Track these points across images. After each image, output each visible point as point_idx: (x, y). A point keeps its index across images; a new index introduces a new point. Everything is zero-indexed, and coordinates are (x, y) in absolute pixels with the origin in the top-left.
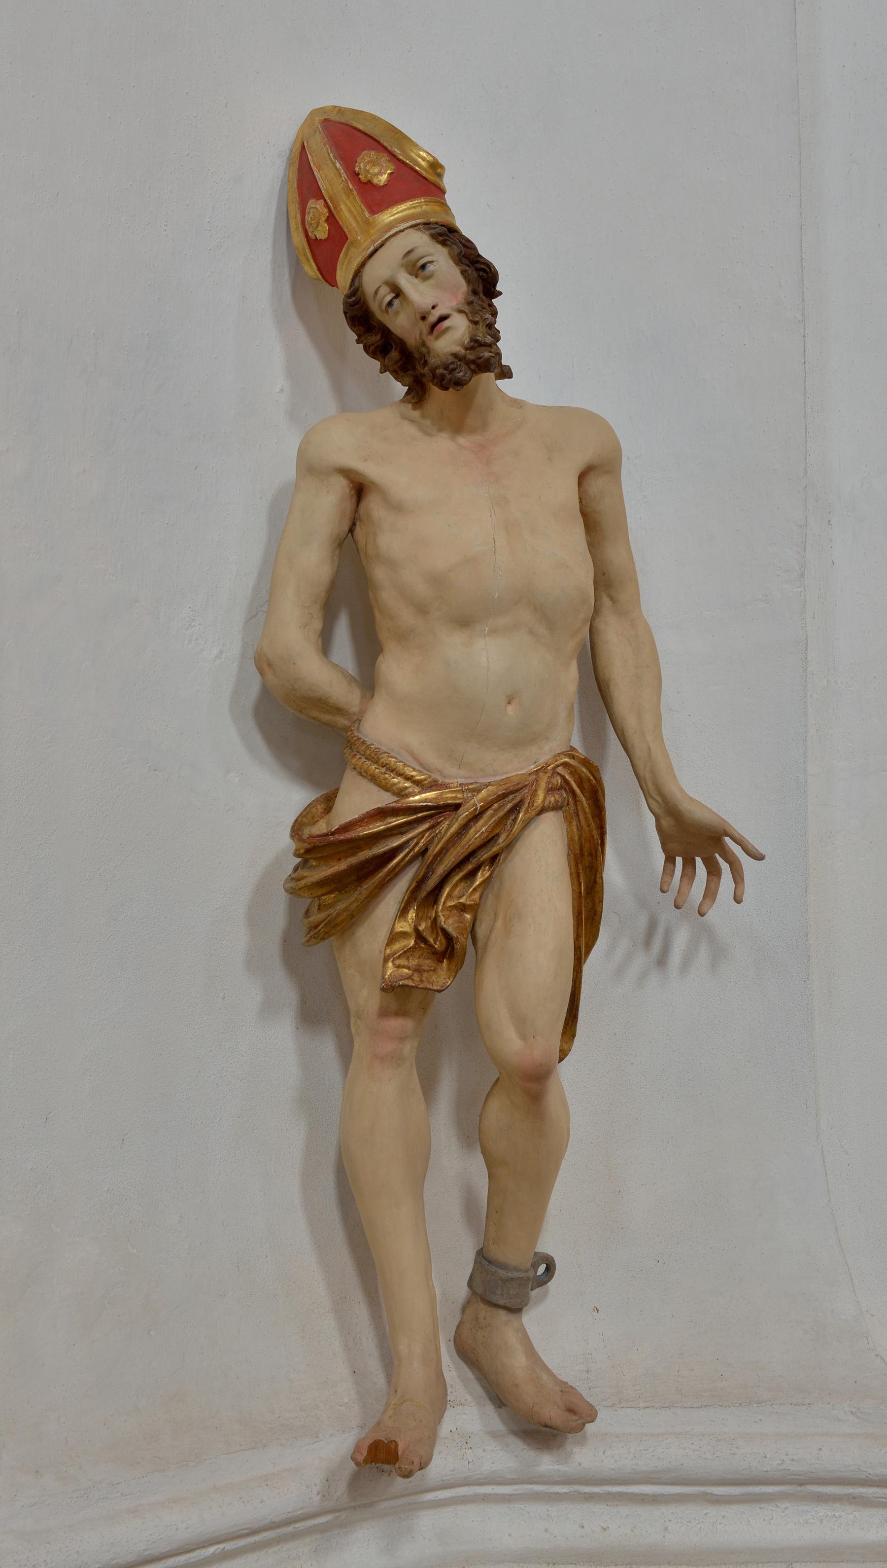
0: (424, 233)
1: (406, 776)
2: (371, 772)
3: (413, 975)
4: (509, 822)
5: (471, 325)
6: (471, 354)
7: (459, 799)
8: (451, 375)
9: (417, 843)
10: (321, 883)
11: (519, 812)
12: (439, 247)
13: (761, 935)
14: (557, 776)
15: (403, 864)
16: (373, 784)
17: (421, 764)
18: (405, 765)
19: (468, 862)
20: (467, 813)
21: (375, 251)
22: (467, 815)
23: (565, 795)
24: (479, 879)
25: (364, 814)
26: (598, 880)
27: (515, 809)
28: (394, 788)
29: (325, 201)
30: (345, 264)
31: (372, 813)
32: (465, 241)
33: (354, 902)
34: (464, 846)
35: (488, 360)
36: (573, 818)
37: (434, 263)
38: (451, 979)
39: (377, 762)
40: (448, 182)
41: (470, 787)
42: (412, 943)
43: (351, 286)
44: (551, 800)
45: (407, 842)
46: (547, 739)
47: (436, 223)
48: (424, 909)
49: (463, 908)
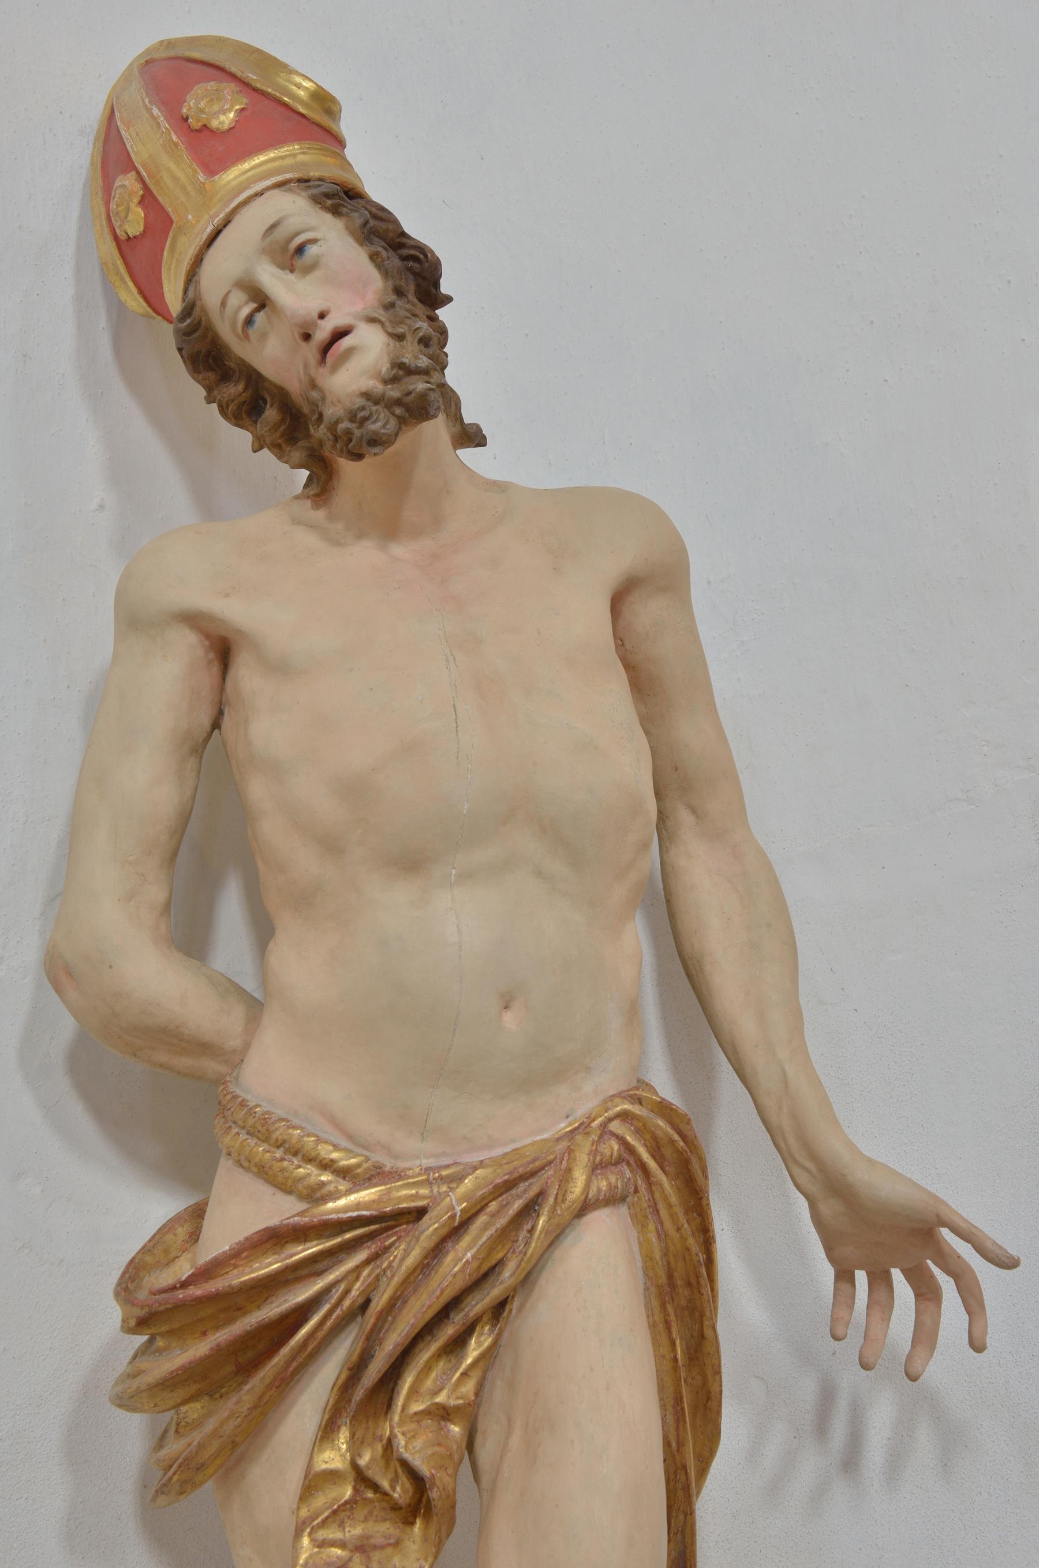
0: (299, 194)
1: (321, 1161)
2: (257, 1159)
3: (350, 1559)
4: (523, 1234)
5: (392, 342)
6: (392, 389)
7: (424, 1197)
8: (362, 430)
9: (347, 1292)
10: (171, 1383)
11: (538, 1216)
12: (328, 217)
13: (1027, 1400)
14: (610, 1139)
15: (320, 1335)
16: (262, 1181)
17: (350, 1137)
18: (319, 1140)
19: (446, 1320)
20: (436, 1225)
21: (217, 233)
22: (436, 1229)
23: (628, 1174)
24: (473, 1350)
25: (240, 1242)
26: (708, 1332)
27: (530, 1209)
28: (300, 1186)
29: (138, 173)
30: (173, 266)
31: (256, 1239)
32: (378, 209)
33: (228, 1419)
34: (434, 1291)
35: (423, 396)
36: (647, 1217)
37: (319, 243)
38: (430, 1560)
39: (266, 1140)
40: (347, 126)
41: (444, 1173)
42: (348, 1493)
43: (184, 301)
44: (601, 1185)
45: (327, 1290)
46: (588, 1069)
47: (320, 179)
48: (368, 1422)
49: (444, 1414)
